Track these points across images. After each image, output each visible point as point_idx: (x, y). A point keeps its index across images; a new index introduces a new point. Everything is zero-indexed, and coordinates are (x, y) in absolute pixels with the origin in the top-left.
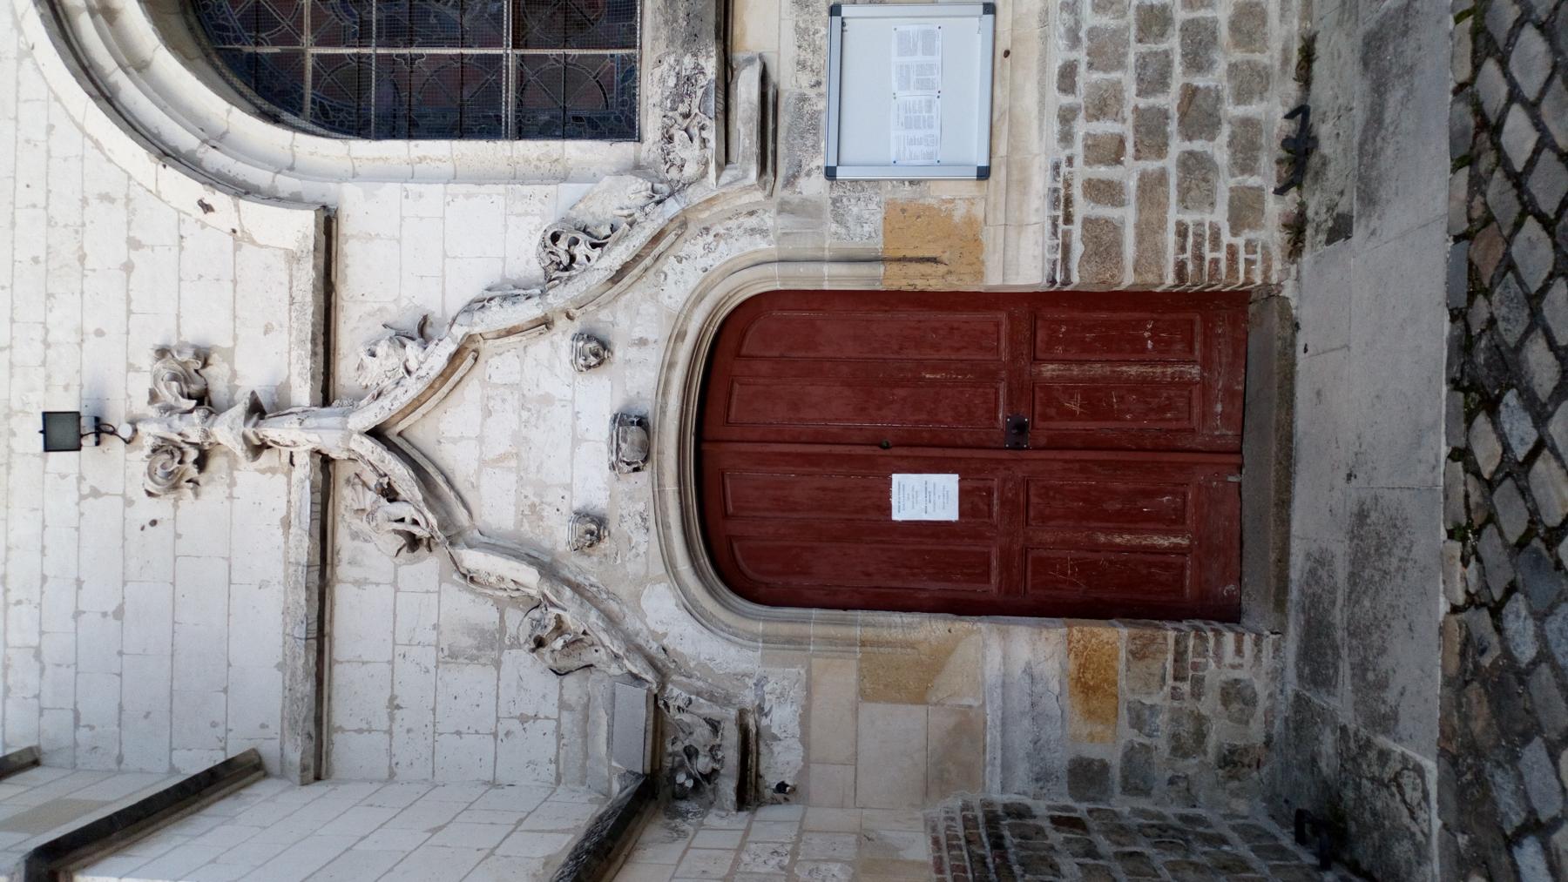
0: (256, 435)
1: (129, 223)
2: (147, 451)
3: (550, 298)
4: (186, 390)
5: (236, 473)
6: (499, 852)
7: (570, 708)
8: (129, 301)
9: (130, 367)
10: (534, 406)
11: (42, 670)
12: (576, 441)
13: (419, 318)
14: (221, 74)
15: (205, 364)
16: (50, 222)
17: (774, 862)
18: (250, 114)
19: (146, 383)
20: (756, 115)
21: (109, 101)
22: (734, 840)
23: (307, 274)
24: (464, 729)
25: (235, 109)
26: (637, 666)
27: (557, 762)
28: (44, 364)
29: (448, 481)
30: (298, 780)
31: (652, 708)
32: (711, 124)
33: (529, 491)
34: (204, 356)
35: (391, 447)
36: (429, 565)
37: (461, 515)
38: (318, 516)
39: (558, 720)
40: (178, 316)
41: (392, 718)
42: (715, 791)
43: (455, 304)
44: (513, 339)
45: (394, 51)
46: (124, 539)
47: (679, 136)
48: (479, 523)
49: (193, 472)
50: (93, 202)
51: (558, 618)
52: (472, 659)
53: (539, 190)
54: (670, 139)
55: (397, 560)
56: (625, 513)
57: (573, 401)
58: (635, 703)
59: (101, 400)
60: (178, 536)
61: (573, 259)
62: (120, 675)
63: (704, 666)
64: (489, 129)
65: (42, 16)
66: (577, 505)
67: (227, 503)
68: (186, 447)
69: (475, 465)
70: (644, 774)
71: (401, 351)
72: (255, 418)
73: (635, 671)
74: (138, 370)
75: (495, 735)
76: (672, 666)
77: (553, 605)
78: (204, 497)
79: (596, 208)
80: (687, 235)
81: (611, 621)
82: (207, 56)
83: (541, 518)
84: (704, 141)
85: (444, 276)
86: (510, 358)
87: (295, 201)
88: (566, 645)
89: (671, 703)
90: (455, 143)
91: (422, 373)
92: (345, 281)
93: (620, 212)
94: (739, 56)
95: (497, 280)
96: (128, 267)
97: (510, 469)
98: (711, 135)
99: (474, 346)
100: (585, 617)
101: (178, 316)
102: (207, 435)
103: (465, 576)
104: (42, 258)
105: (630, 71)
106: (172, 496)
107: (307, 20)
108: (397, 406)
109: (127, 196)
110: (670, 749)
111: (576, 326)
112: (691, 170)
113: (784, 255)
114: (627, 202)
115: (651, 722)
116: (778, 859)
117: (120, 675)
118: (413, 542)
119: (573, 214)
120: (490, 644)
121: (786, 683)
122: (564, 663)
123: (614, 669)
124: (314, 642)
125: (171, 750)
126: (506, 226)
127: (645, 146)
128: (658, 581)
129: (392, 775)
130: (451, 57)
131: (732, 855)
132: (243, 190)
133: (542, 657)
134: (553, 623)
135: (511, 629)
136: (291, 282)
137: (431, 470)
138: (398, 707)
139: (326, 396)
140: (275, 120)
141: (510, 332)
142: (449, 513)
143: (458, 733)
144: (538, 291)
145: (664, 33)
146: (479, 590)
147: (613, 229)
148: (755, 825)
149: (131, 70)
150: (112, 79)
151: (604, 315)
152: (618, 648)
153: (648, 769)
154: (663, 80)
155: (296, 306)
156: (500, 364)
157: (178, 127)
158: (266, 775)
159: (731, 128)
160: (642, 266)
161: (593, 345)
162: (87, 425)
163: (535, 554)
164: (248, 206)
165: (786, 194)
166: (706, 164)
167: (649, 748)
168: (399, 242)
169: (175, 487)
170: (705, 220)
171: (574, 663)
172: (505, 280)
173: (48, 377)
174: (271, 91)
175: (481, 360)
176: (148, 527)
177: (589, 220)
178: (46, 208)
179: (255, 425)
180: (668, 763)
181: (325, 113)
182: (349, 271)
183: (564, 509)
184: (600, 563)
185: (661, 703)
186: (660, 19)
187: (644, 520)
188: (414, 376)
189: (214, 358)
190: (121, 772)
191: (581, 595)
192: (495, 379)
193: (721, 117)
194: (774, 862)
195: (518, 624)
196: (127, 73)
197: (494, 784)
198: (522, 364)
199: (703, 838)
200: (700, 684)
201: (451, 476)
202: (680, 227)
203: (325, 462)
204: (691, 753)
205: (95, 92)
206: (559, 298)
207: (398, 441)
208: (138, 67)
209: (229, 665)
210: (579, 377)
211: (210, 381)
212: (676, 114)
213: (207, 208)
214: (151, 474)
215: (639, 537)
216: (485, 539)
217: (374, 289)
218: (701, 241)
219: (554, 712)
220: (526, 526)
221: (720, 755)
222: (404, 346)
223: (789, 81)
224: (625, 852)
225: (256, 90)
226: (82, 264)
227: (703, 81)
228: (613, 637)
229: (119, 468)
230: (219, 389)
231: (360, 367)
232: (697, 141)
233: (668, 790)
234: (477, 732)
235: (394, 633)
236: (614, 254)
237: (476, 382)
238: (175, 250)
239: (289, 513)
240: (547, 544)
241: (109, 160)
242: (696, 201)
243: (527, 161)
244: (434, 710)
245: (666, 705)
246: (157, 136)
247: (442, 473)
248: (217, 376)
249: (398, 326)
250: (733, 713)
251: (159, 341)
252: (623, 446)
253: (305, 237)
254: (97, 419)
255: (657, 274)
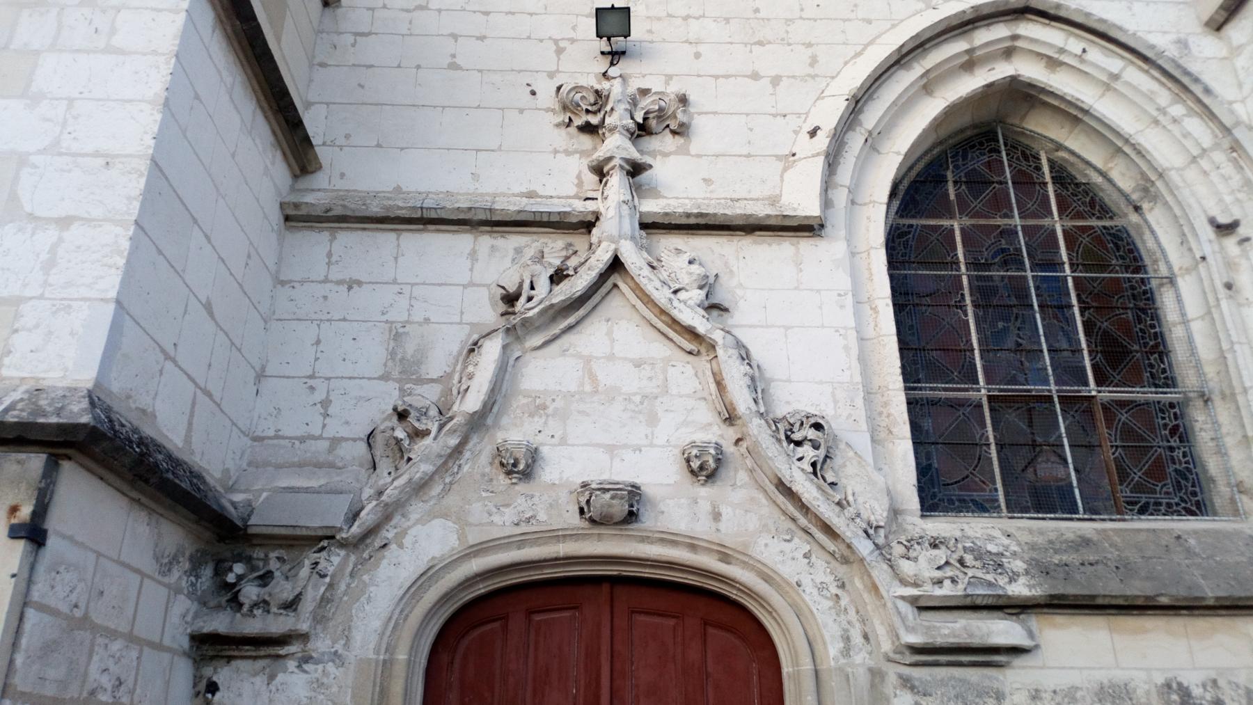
0: (612, 169)
1: (794, 77)
2: (598, 87)
3: (757, 421)
4: (651, 116)
5: (577, 156)
6: (169, 365)
7: (331, 450)
8: (727, 77)
9: (669, 78)
10: (646, 407)
11: (408, 11)
12: (611, 449)
13: (726, 305)
14: (926, 153)
15: (674, 133)
16: (789, 21)
17: (106, 681)
18: (897, 173)
19: (655, 85)
20: (976, 641)
21: (897, 62)
22: (147, 627)
23: (761, 210)
24: (321, 347)
25: (900, 158)
26: (368, 516)
27: (277, 437)
28: (669, 16)
29: (570, 328)
30: (287, 200)
31: (320, 533)
32: (959, 590)
33: (559, 403)
34: (681, 131)
35: (603, 277)
36: (488, 313)
37: (537, 340)
38: (538, 219)
39: (320, 438)
40: (715, 113)
41: (339, 283)
42: (219, 607)
43: (745, 336)
44: (713, 387)
45: (966, 292)
46: (520, 71)
47: (941, 555)
48: (528, 356)
49: (578, 121)
50: (810, 51)
51: (426, 433)
52: (393, 354)
53: (861, 414)
54: (934, 546)
55: (494, 286)
56: (536, 500)
57: (652, 445)
58: (330, 514)
59: (639, 56)
60: (521, 111)
61: (798, 444)
62: (399, 66)
63: (363, 592)
64: (909, 374)
65: (964, 12)
66: (545, 450)
67: (551, 149)
68: (600, 116)
69: (585, 353)
70: (247, 526)
71: (695, 285)
72: (628, 167)
73: (363, 514)
74: (667, 83)
75: (312, 377)
76: (366, 555)
77: (441, 427)
78: (556, 131)
79: (851, 469)
80: (834, 564)
81: (420, 487)
82: (941, 143)
83: (531, 415)
84: (939, 582)
85: (767, 327)
86: (694, 384)
87: (827, 203)
88: (398, 442)
89: (324, 554)
90: (895, 339)
91: (676, 303)
92: (755, 243)
93: (849, 493)
94: (1034, 621)
95: (768, 375)
96: (755, 76)
97: (582, 384)
98: (947, 590)
99: (703, 350)
100: (426, 459)
101: (715, 113)
102: (612, 130)
103: (476, 344)
104: (758, 15)
105: (983, 507)
106: (557, 107)
107: (982, 222)
108: (643, 282)
109: (817, 76)
110: (273, 555)
111: (729, 448)
112: (907, 567)
113: (824, 676)
114: (860, 500)
115: (304, 532)
116: (109, 687)
117: (399, 66)
118: (510, 299)
119: (842, 446)
120: (406, 369)
121: (335, 689)
122: (379, 440)
123: (368, 492)
124: (418, 215)
125: (327, 104)
126: (821, 383)
127: (919, 521)
128: (462, 537)
129: (283, 283)
130: (969, 341)
131: (124, 628)
132: (832, 160)
133: (389, 418)
134: (421, 426)
135: (419, 389)
136: (752, 199)
137: (582, 312)
138: (350, 288)
139: (650, 226)
140: (893, 194)
141: (720, 384)
142: (538, 329)
143: (318, 342)
144: (762, 410)
145: (1040, 540)
146: (461, 359)
147: (833, 484)
148: (166, 656)
149: (925, 80)
150: (915, 65)
151: (742, 476)
152: (390, 494)
153: (251, 531)
154: (991, 539)
155: (730, 203)
156: (687, 376)
157: (880, 113)
158: (295, 177)
159: (956, 614)
160: (797, 514)
161: (712, 464)
162: (619, 43)
163: (495, 409)
164: (819, 164)
165: (892, 679)
166: (916, 585)
167: (276, 531)
168: (796, 288)
169: (565, 108)
170: (852, 583)
171: (379, 451)
172: (768, 382)
173: (659, 19)
174: (916, 192)
175: (690, 358)
176: (530, 89)
177: (838, 461)
178: (801, 18)
179: (621, 167)
180: (258, 553)
181: (901, 235)
182: (765, 247)
183: (540, 438)
184: (483, 475)
185: (325, 543)
186: (1053, 536)
187: (528, 520)
188: (672, 296)
189: (679, 140)
190: (311, 66)
191: (450, 456)
192: (671, 370)
193: (968, 602)
194: (106, 681)
195: (426, 396)
196: (922, 76)
197: (261, 376)
198: (688, 396)
199: (155, 594)
200: (343, 587)
201: (575, 331)
202: (842, 556)
203: (587, 225)
204: (265, 579)
205: (904, 50)
206: (757, 429)
207: (609, 284)
208: (928, 86)
209: (402, 149)
210: (677, 451)
211: (659, 137)
212: (960, 553)
213: (813, 133)
214: (577, 89)
215: (509, 515)
216: (511, 362)
217: (747, 266)
218: (829, 579)
219: (329, 433)
220: (524, 401)
221: (258, 612)
222: (701, 288)
223: (1015, 679)
224: (143, 499)
225: (914, 182)
226: (755, 43)
227: (1002, 581)
228: (402, 490)
229: (583, 66)
230: (652, 143)
231: (678, 251)
232: (938, 574)
233: (228, 554)
234: (317, 359)
235: (424, 284)
236: (807, 484)
237: (669, 353)
238: (773, 111)
239: (541, 197)
240: (505, 421)
241: (846, 63)
242: (875, 573)
243: (886, 404)
244: (344, 320)
245: (323, 548)
246: (871, 98)
247: (578, 323)
248: (665, 142)
249: (718, 287)
250: (304, 627)
251: (692, 98)
252: (608, 496)
253: (795, 210)
254: (624, 53)
255: (789, 531)
